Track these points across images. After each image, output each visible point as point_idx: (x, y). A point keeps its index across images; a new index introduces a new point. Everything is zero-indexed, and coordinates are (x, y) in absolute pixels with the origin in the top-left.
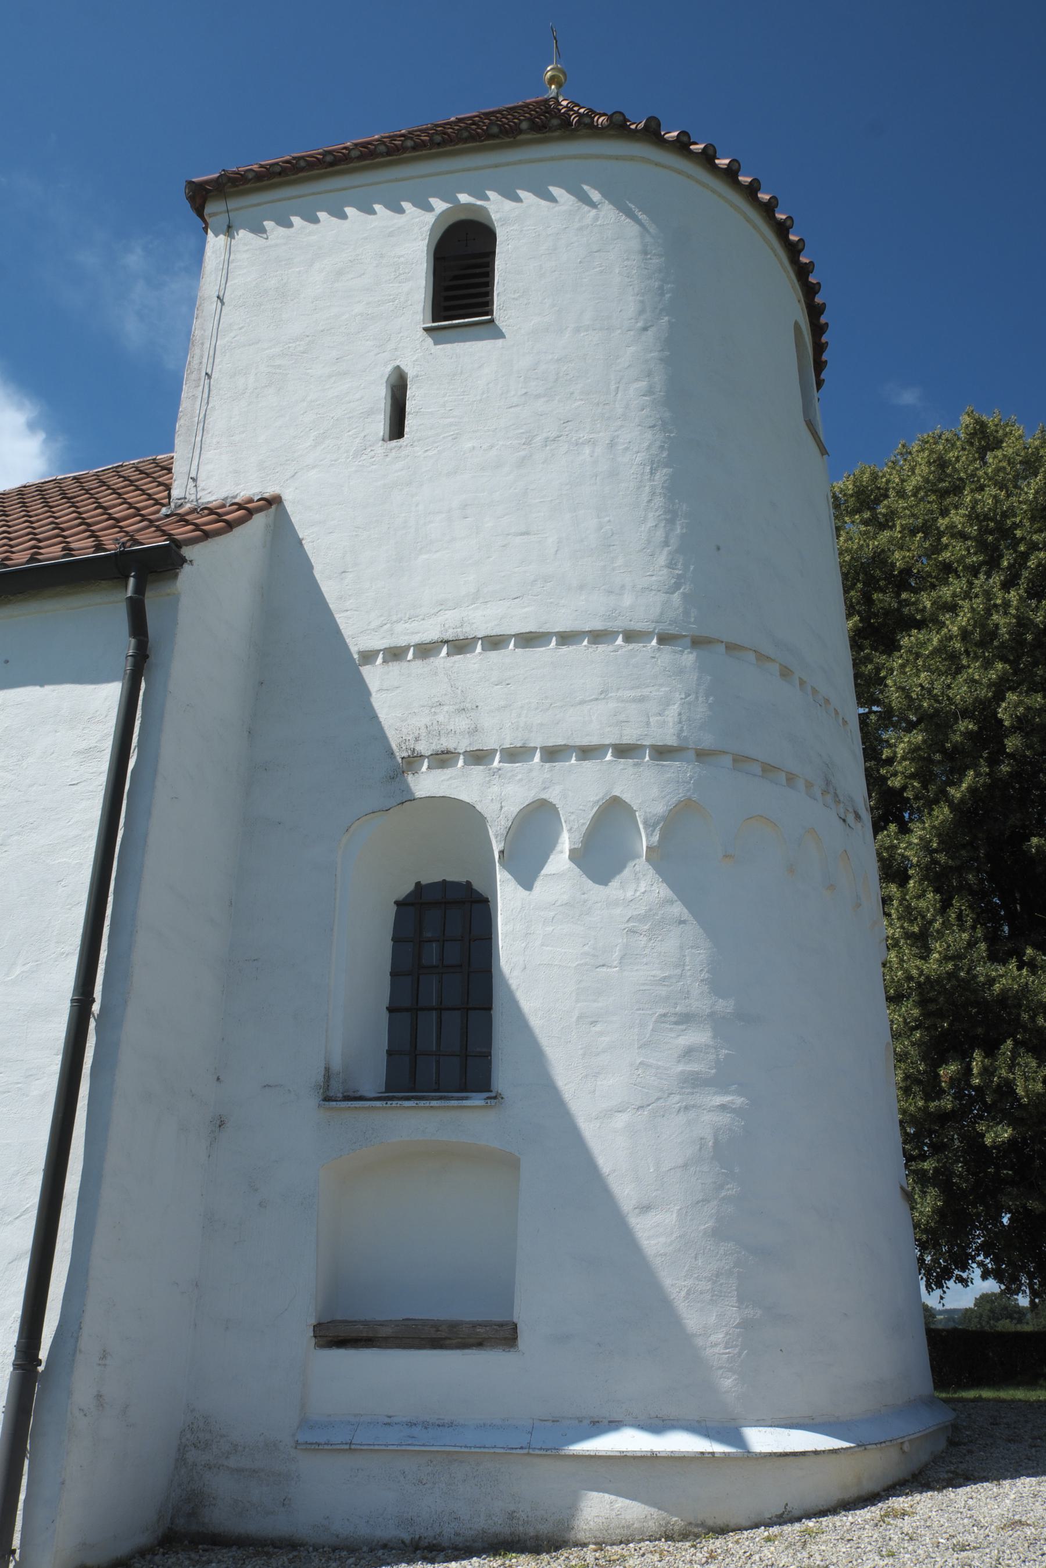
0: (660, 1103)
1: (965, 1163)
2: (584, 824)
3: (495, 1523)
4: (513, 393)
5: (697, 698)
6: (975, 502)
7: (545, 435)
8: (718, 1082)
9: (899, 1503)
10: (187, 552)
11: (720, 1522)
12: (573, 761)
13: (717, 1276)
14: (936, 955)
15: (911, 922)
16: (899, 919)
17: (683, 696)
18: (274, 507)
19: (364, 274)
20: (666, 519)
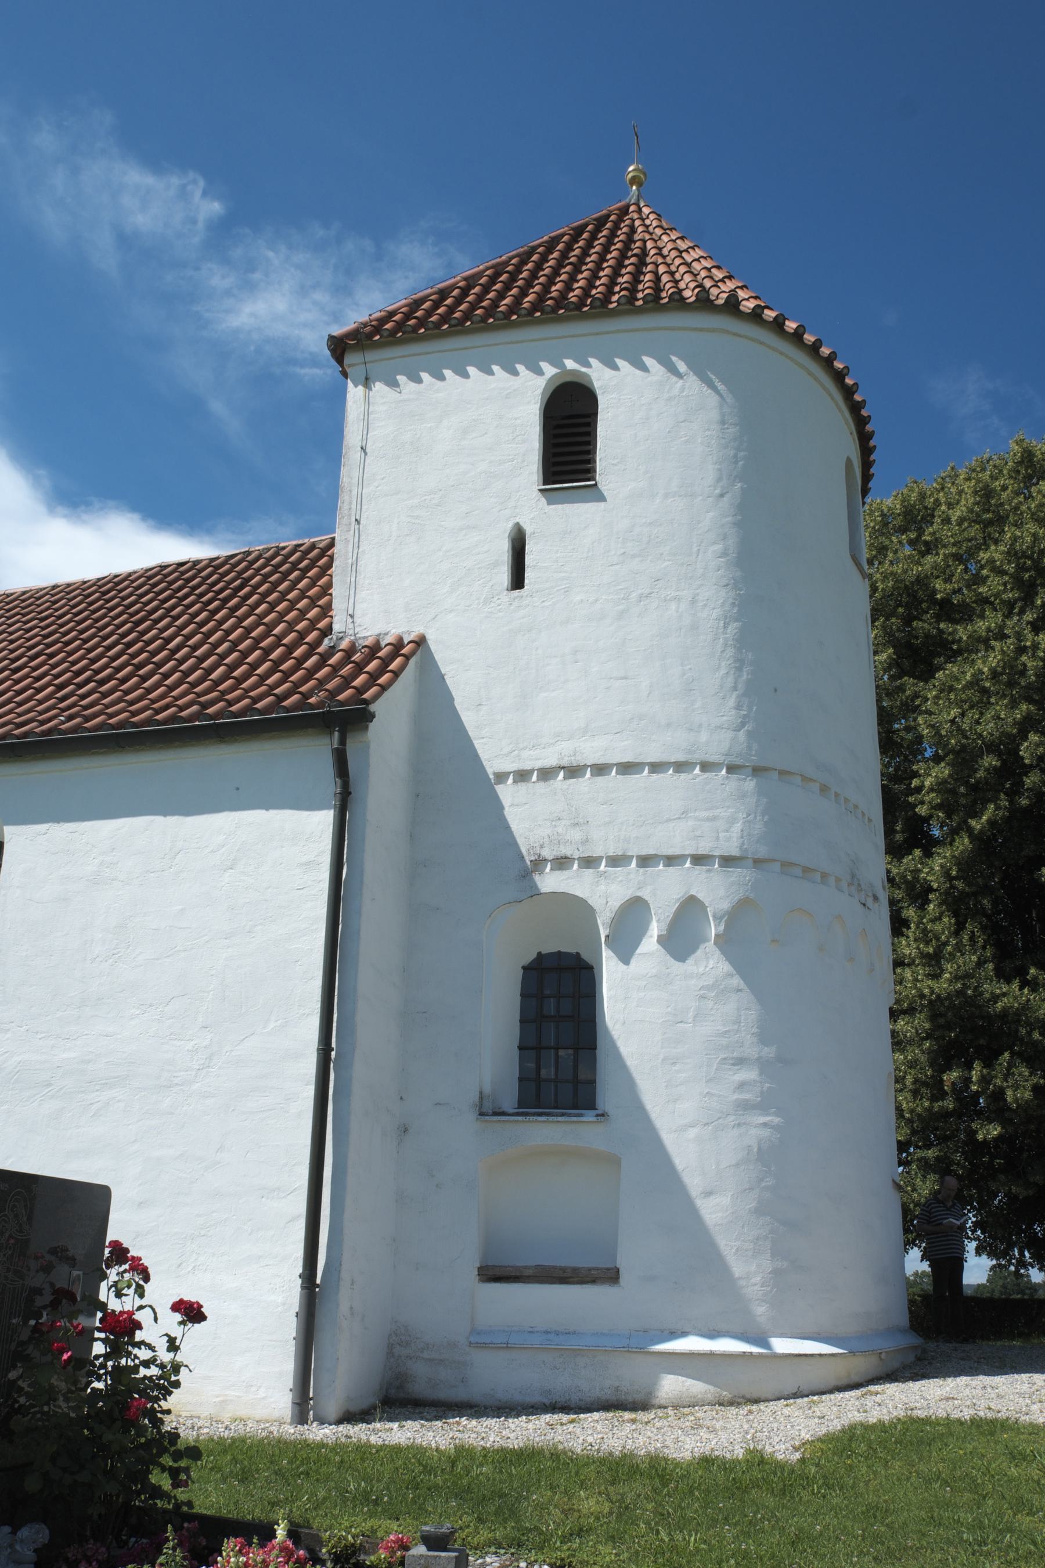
0: (720, 1121)
1: (963, 1153)
2: (668, 916)
3: (607, 1394)
4: (613, 553)
5: (755, 817)
6: (1015, 539)
7: (640, 592)
8: (762, 1106)
9: (872, 1388)
10: (372, 708)
11: (755, 1396)
12: (661, 867)
13: (757, 1239)
14: (947, 975)
15: (927, 943)
16: (915, 940)
17: (745, 816)
19: (486, 433)
20: (736, 668)
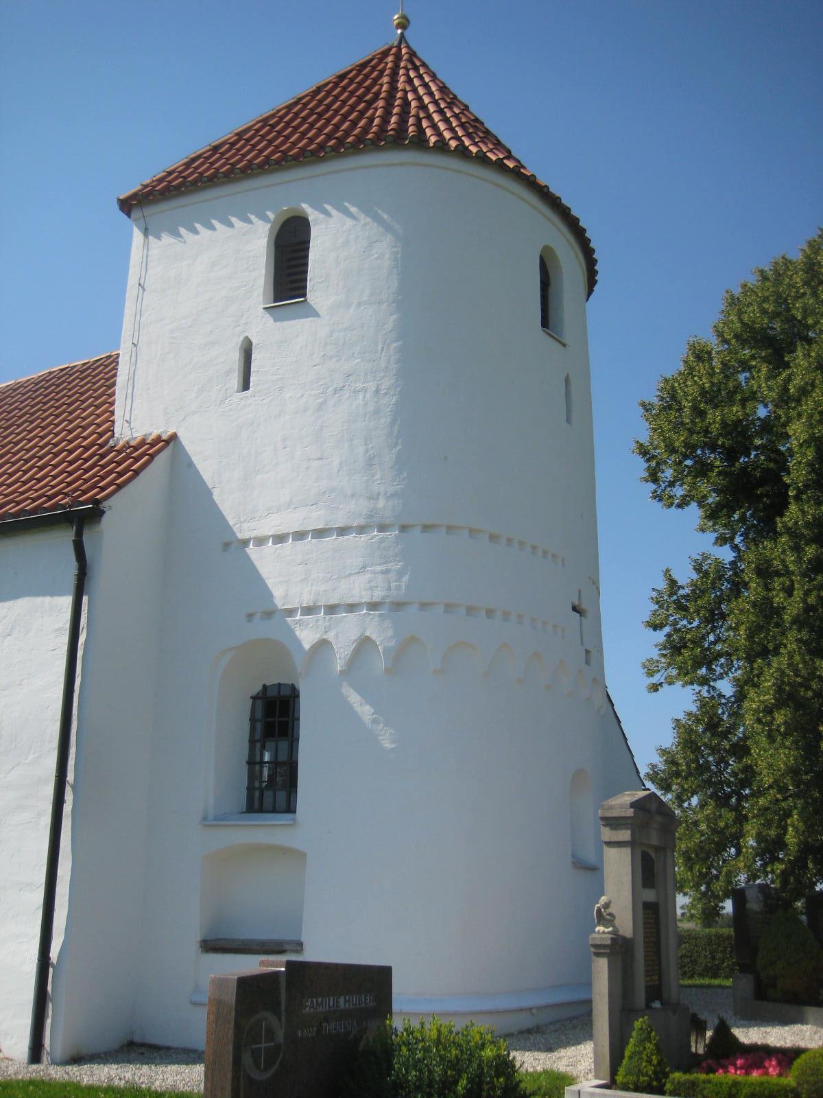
18: (171, 444)
